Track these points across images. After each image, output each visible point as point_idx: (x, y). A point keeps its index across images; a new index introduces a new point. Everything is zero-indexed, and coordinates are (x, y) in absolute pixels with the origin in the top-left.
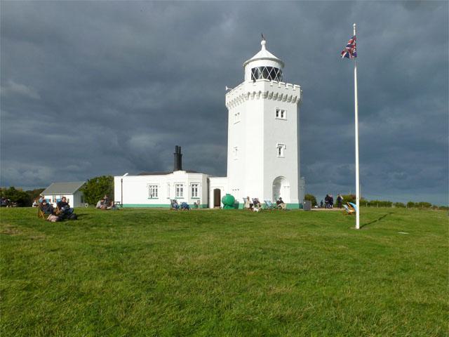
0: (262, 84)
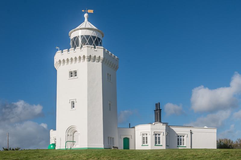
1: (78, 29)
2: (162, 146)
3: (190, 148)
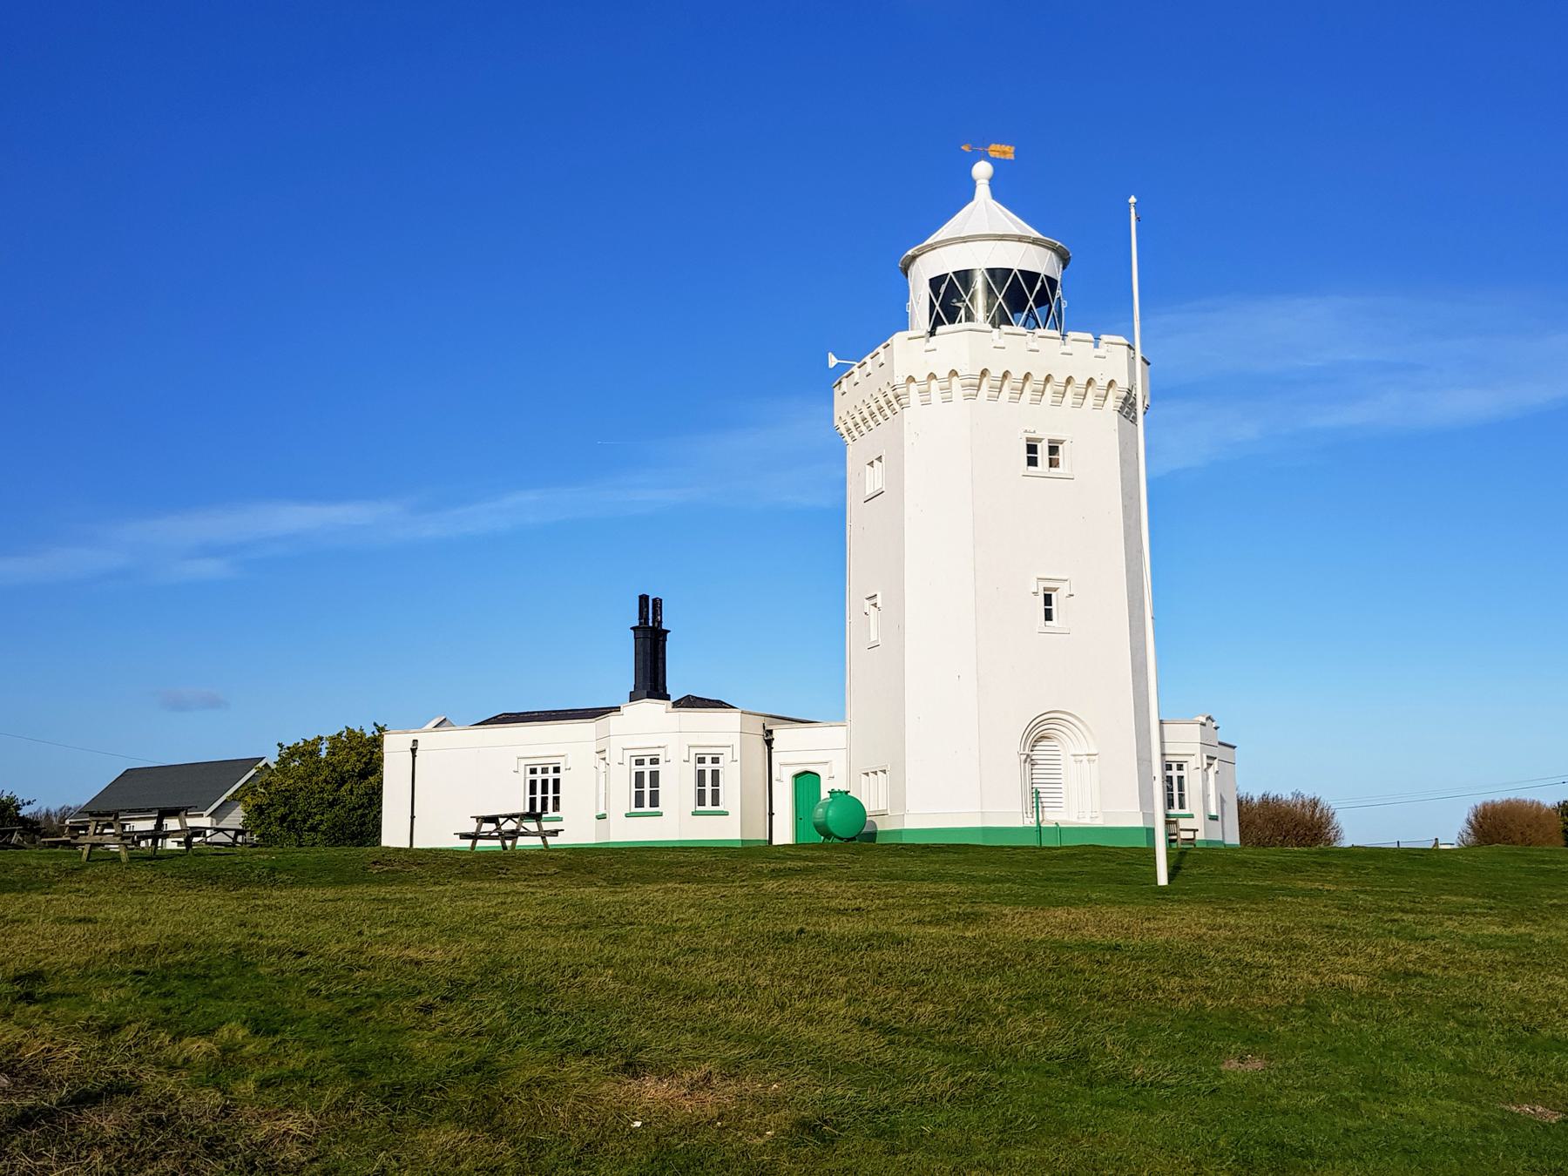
0: (975, 342)
1: (933, 247)
2: (1191, 816)
3: (407, 845)
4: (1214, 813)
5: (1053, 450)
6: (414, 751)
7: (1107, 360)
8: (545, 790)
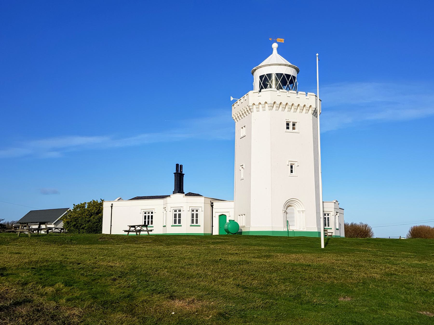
0: (272, 94)
2: (331, 229)
4: (337, 228)
5: (294, 125)
6: (112, 207)
7: (310, 100)
8: (149, 219)
